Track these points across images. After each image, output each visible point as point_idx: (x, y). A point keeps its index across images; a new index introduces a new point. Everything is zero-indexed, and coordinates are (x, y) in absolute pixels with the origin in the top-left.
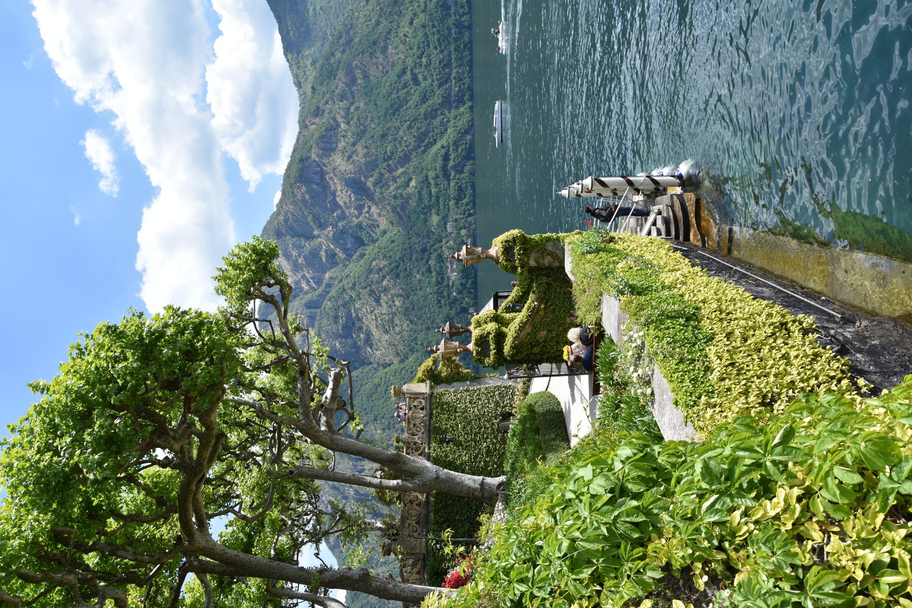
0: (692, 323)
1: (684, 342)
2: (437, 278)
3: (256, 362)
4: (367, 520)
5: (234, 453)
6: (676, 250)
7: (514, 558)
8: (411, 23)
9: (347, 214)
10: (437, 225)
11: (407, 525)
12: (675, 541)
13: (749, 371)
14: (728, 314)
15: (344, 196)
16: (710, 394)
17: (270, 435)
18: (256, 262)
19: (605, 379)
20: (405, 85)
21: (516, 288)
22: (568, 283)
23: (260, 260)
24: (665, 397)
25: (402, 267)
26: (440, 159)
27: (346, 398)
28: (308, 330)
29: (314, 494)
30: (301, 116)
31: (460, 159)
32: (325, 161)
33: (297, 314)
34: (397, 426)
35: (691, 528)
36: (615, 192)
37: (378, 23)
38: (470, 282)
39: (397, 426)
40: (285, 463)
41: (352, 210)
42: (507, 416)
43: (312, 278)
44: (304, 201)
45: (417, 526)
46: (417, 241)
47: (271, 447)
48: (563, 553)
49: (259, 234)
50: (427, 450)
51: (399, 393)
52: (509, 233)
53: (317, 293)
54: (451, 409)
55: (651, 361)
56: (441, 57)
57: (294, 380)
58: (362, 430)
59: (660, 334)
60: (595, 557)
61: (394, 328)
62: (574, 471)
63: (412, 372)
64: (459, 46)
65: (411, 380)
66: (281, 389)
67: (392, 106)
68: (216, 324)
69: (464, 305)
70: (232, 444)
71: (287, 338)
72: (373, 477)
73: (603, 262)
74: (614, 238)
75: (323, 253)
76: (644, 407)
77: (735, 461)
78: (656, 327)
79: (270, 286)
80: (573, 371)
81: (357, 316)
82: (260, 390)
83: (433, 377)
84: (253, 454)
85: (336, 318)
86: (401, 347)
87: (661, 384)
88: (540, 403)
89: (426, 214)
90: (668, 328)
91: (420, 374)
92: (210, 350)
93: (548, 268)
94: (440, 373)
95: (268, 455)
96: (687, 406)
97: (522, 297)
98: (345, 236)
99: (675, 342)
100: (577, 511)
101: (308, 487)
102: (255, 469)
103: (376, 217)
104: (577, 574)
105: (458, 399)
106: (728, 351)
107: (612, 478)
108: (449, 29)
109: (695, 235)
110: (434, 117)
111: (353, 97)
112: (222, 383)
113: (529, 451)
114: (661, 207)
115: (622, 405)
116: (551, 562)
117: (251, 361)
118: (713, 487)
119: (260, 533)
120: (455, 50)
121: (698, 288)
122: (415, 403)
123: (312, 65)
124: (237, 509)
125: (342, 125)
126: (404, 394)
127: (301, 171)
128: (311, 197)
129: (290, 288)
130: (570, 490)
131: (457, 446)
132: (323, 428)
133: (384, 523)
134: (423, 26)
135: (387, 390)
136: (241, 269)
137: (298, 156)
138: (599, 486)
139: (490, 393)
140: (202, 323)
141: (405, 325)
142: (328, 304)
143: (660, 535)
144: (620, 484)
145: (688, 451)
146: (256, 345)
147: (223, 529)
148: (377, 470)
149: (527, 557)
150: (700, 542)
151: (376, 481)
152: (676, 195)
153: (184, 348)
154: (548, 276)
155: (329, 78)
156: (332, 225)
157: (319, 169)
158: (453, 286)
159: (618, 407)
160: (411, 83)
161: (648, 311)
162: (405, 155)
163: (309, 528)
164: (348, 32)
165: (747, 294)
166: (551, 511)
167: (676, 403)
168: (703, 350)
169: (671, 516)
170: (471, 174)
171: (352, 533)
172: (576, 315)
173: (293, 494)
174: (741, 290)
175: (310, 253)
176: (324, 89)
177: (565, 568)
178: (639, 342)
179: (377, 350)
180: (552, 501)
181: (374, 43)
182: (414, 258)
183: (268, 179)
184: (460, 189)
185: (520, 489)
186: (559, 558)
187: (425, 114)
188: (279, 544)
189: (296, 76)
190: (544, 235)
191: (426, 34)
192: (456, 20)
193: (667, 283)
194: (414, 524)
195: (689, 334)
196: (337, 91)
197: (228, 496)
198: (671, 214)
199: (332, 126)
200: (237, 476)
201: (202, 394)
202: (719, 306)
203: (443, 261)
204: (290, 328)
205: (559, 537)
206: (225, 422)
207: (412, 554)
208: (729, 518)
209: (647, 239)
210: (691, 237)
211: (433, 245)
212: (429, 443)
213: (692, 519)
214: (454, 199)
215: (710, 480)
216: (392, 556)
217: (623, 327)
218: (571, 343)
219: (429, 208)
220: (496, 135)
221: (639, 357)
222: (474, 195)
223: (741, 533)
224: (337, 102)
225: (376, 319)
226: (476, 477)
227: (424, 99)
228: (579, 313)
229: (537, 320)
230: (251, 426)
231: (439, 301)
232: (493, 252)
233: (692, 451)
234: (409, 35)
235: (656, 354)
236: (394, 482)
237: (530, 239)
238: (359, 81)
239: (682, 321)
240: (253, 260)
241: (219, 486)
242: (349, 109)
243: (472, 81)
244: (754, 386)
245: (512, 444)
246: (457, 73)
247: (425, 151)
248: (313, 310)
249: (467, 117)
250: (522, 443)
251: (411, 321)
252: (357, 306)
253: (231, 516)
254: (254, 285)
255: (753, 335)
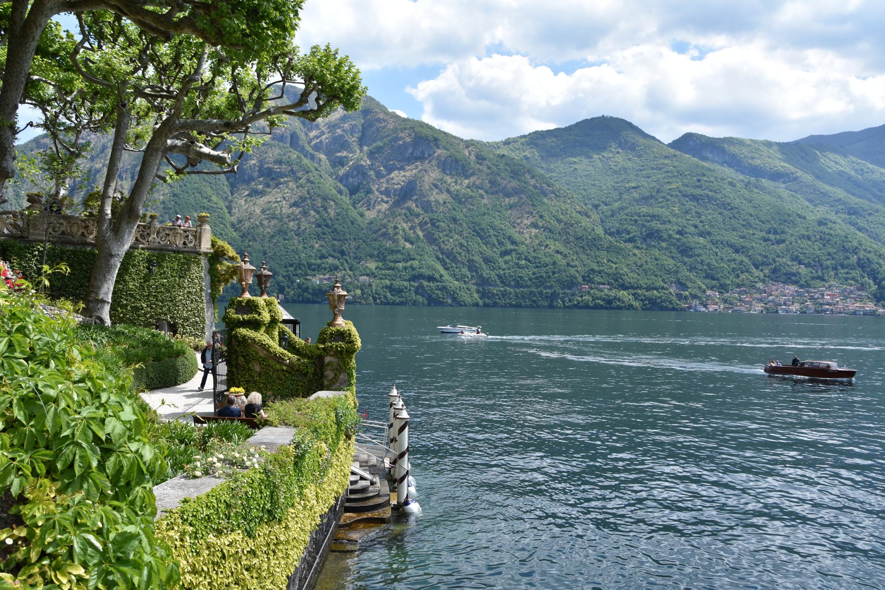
0: (266, 516)
1: (247, 508)
2: (314, 264)
3: (241, 80)
4: (67, 181)
5: (147, 48)
6: (337, 499)
7: (37, 338)
8: (558, 252)
9: (381, 180)
10: (367, 267)
11: (62, 221)
12: (52, 507)
13: (217, 573)
14: (274, 552)
15: (399, 178)
16: (195, 535)
17: (164, 87)
18: (341, 88)
19: (210, 429)
20: (501, 243)
21: (303, 342)
22: (307, 394)
23: (343, 92)
24: (192, 490)
25: (326, 230)
26: (430, 273)
27: (199, 167)
28: (270, 133)
29: (99, 127)
30: (478, 142)
31: (429, 292)
32: (434, 162)
33: (286, 123)
34: (166, 216)
35: (67, 524)
36: (393, 440)
37: (559, 221)
38: (310, 296)
39: (166, 216)
40: (134, 100)
41: (385, 185)
42: (173, 328)
43: (321, 141)
44: (396, 139)
45: (60, 232)
46: (352, 246)
47: (152, 87)
48: (42, 390)
49: (369, 93)
50: (141, 246)
51: (202, 221)
52: (358, 337)
53: (306, 145)
54: (183, 271)
55: (230, 476)
56: (526, 279)
57: (220, 116)
58: (165, 181)
59: (256, 485)
60: (37, 423)
61: (267, 219)
62: (129, 402)
63: (221, 234)
64: (535, 296)
65: (214, 233)
66: (211, 102)
67: (482, 229)
68: (284, 44)
69: (287, 289)
70: (157, 47)
71: (264, 113)
72: (115, 189)
73: (328, 428)
74: (350, 439)
75: (345, 154)
76: (182, 468)
77: (137, 566)
78: (262, 481)
79: (317, 100)
80: (219, 397)
81: (281, 183)
82: (212, 81)
83: (217, 256)
84: (145, 68)
85: (280, 162)
86: (247, 225)
87: (206, 486)
88: (186, 363)
89: (378, 256)
90: (261, 492)
91: (220, 243)
92: (257, 35)
93: (322, 374)
94: (221, 263)
95: (144, 83)
96: (183, 513)
97: (294, 348)
98: (360, 177)
99: (248, 500)
100: (86, 405)
101: (107, 121)
102: (130, 68)
103: (378, 207)
104: (18, 404)
105: (193, 280)
106: (237, 552)
107: (122, 440)
108: (551, 287)
109: (350, 517)
110: (470, 269)
111: (493, 193)
112: (223, 43)
113: (136, 350)
114: (378, 485)
115: (183, 446)
116: (31, 376)
117: (243, 75)
118: (110, 545)
119: (60, 66)
120: (532, 292)
121: (300, 522)
122: (190, 237)
123: (525, 156)
124: (87, 45)
125: (467, 181)
126: (200, 226)
127: (426, 139)
128: (400, 146)
129: (314, 120)
130: (109, 398)
131: (144, 278)
132: (169, 142)
133: (64, 198)
134: (554, 263)
135: (204, 208)
136: (335, 72)
137: (440, 137)
138: (113, 427)
139: (199, 313)
140: (285, 29)
141: (269, 230)
142: (294, 155)
143: (60, 492)
144: (115, 448)
145: (146, 517)
146: (259, 80)
147: (64, 27)
148: (122, 193)
149: (38, 352)
150: (51, 533)
151: (111, 192)
152: (389, 500)
153: (261, 10)
154: (315, 374)
155: (512, 172)
156: (372, 165)
157: (426, 155)
158: (306, 279)
159: (182, 442)
160: (503, 249)
161: (279, 472)
162: (436, 240)
163: (62, 118)
164: (553, 192)
165: (293, 570)
166: (87, 377)
167: (185, 501)
168: (239, 527)
169: (79, 502)
170: (415, 301)
171: (55, 163)
172: (276, 401)
173: (99, 105)
174: (297, 564)
175: (346, 141)
176: (501, 166)
177: (25, 392)
178: (248, 463)
179: (245, 201)
180: (98, 378)
181: (541, 217)
182: (335, 242)
183: (419, 107)
184: (400, 291)
185: (96, 340)
186: (37, 385)
187: (473, 261)
188: (45, 85)
189: (515, 140)
190: (354, 371)
191: (547, 265)
192: (559, 294)
193: (305, 491)
194: (61, 229)
195: (254, 513)
196: (499, 179)
197: (100, 36)
198: (371, 494)
199: (467, 171)
200: (123, 49)
201: (213, 22)
202: (281, 542)
203: (331, 270)
204: (274, 116)
205: (60, 386)
206: (180, 43)
207: (28, 225)
208: (76, 562)
209: (347, 472)
210: (348, 514)
211: (347, 262)
212: (148, 249)
213: (76, 523)
214: (391, 284)
215: (118, 541)
216: (26, 204)
217: (263, 447)
218: (247, 396)
219: (383, 260)
220: (448, 327)
221: (233, 464)
222: (394, 304)
223: (59, 577)
224: (489, 177)
225: (276, 202)
226: (110, 295)
227: (487, 260)
228: (277, 404)
229: (272, 362)
230: (175, 69)
231: (291, 265)
232: (340, 321)
233: (147, 521)
234: (547, 250)
235: (236, 481)
236: (108, 211)
237: (351, 358)
238: (507, 200)
239: (268, 506)
240: (343, 86)
241: (113, 29)
242: (482, 188)
243: (502, 306)
244: (201, 579)
245: (144, 333)
246: (510, 293)
247: (438, 258)
248: (289, 140)
249: (469, 300)
250: (145, 343)
251: (273, 236)
252: (291, 184)
253: (78, 38)
254: (319, 84)
255: (252, 577)
